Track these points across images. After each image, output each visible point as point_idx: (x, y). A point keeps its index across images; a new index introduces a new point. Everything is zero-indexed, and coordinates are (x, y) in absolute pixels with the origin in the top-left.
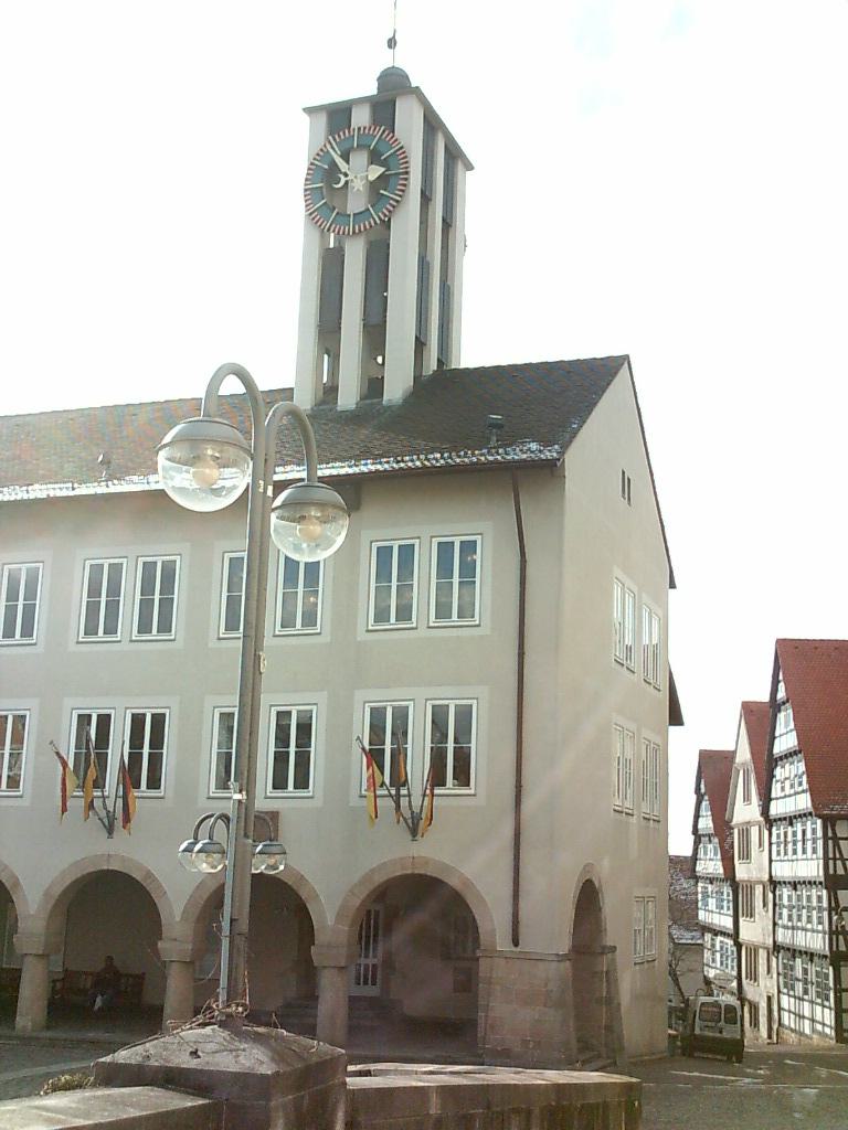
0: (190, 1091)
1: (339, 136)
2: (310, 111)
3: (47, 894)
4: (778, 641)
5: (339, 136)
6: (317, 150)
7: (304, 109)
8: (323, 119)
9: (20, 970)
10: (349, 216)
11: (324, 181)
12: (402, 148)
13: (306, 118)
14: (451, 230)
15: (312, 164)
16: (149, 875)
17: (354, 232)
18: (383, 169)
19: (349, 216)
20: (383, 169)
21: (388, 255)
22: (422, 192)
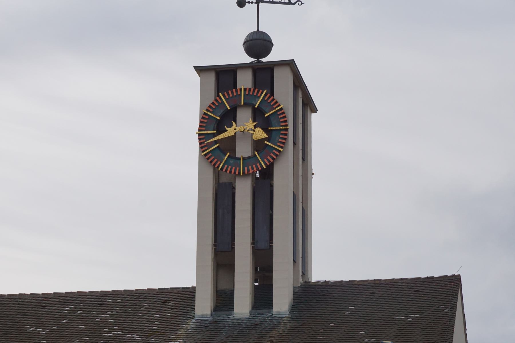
0: (175, 291)
1: (228, 94)
2: (200, 70)
4: (459, 275)
5: (228, 94)
6: (209, 103)
7: (194, 67)
8: (212, 78)
9: (232, 291)
10: (239, 159)
11: (215, 122)
12: (281, 109)
13: (196, 79)
14: (305, 162)
15: (205, 114)
17: (244, 173)
18: (265, 136)
19: (239, 159)
20: (265, 136)
21: (271, 216)
22: (294, 142)
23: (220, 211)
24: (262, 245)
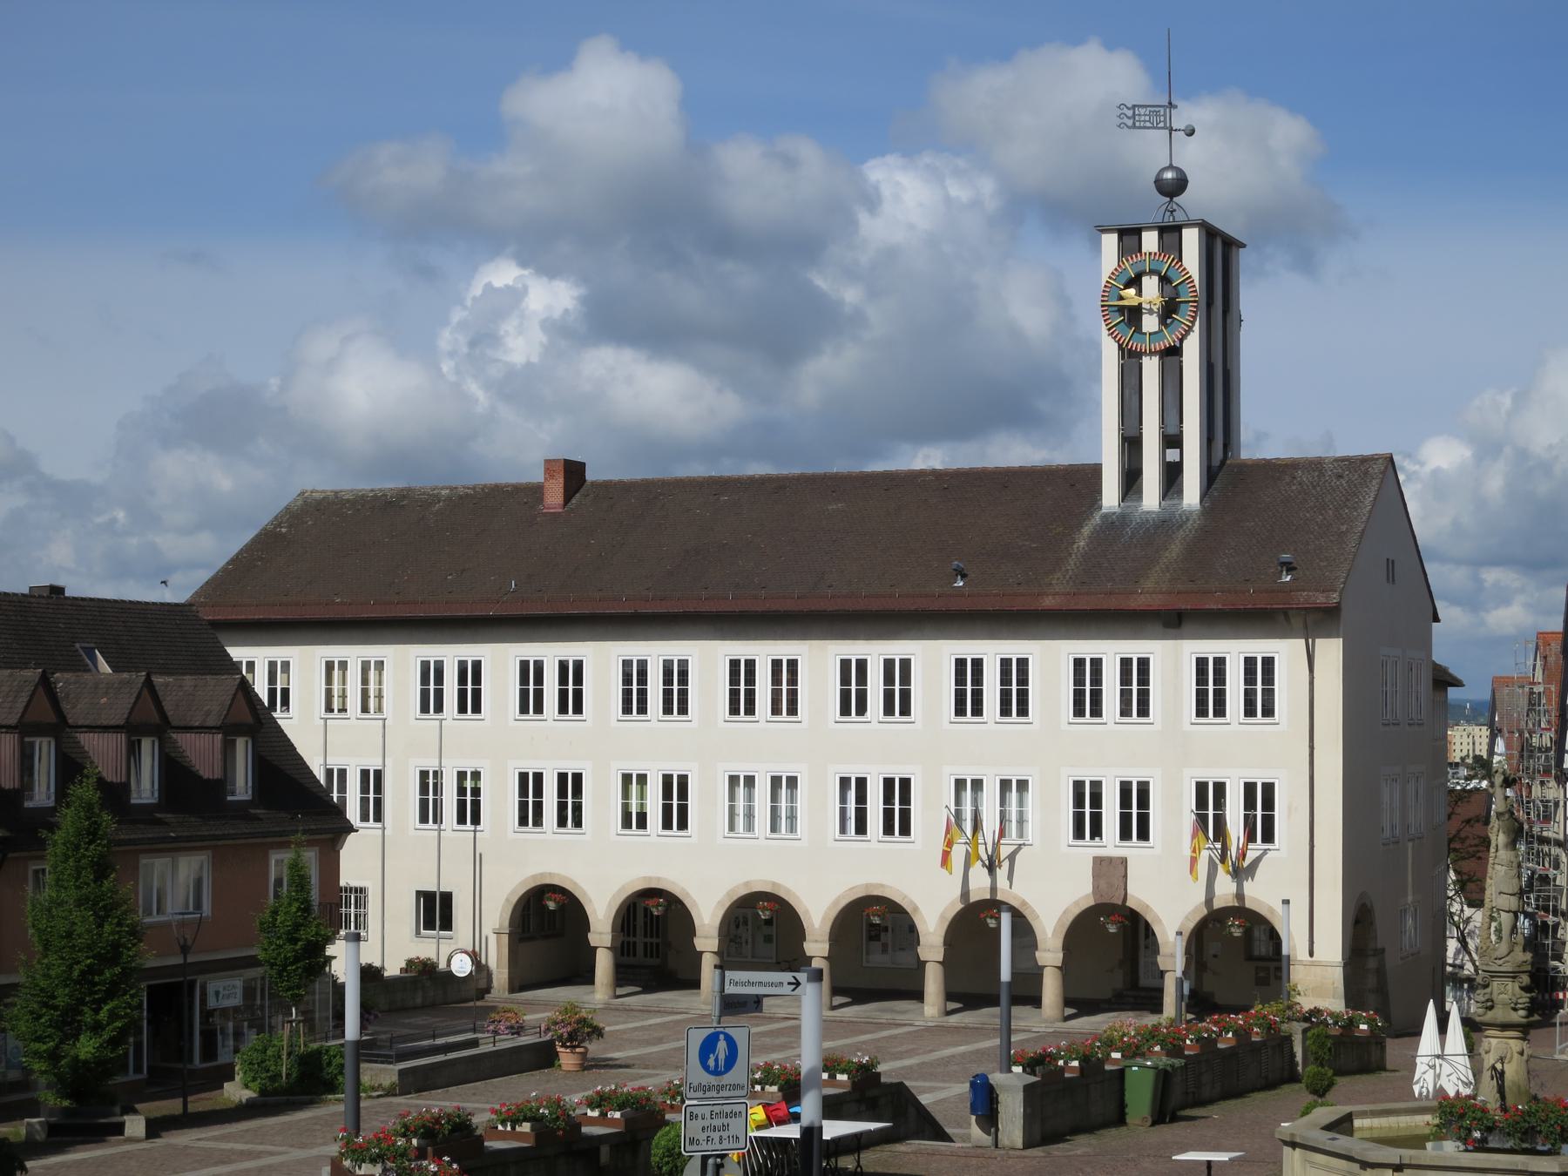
3: (942, 917)
16: (1024, 903)
23: (1127, 392)
24: (1172, 431)
